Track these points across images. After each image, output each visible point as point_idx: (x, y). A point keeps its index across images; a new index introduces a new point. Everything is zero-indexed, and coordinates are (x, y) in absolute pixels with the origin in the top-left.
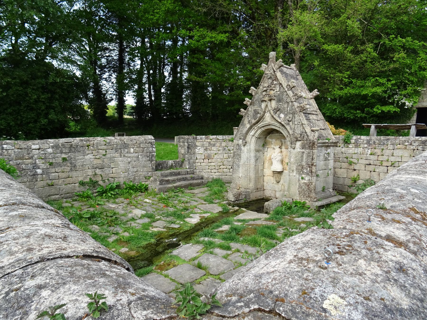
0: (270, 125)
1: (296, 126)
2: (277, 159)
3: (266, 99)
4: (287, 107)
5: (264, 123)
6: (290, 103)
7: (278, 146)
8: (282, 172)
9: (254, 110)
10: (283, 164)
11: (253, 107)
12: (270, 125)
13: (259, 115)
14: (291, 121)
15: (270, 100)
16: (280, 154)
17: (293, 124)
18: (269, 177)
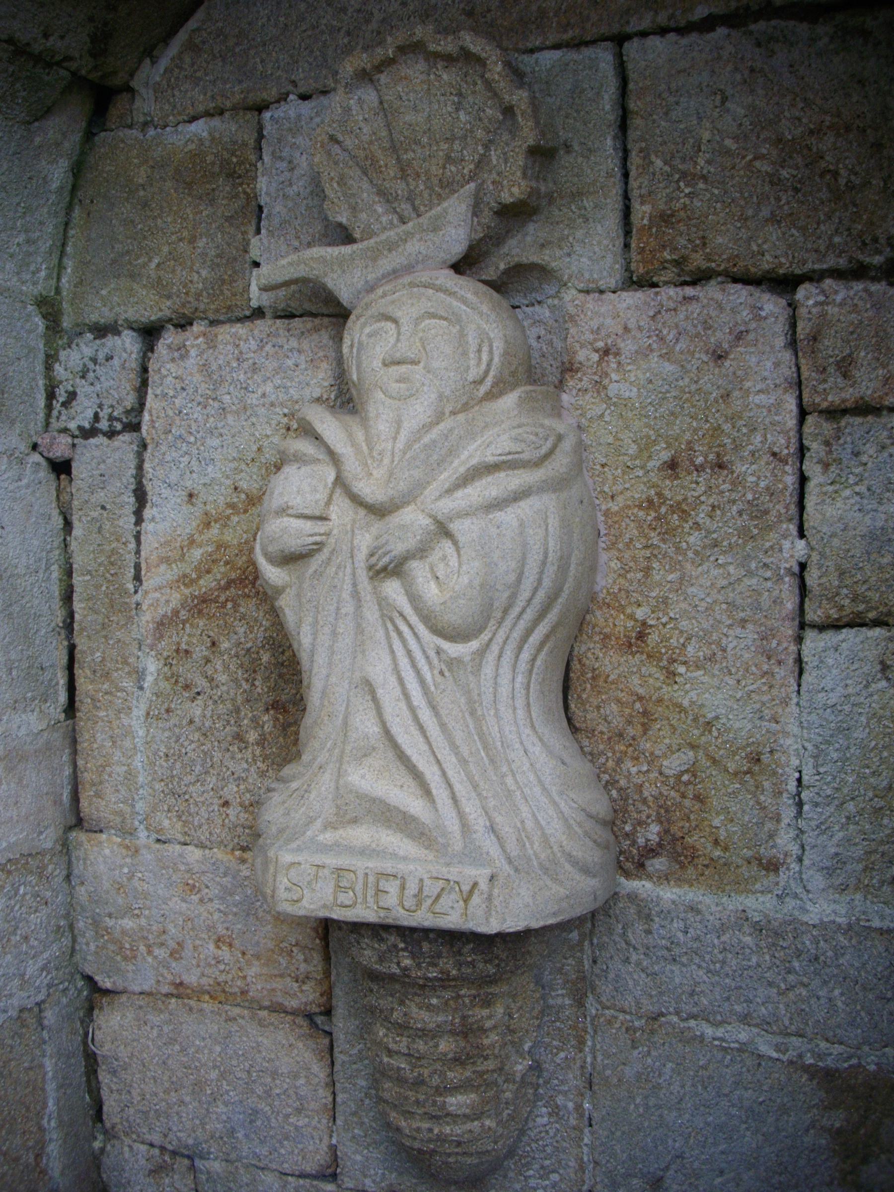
2: (446, 581)
7: (454, 225)
8: (586, 927)
10: (606, 712)
16: (506, 424)
18: (201, 1028)
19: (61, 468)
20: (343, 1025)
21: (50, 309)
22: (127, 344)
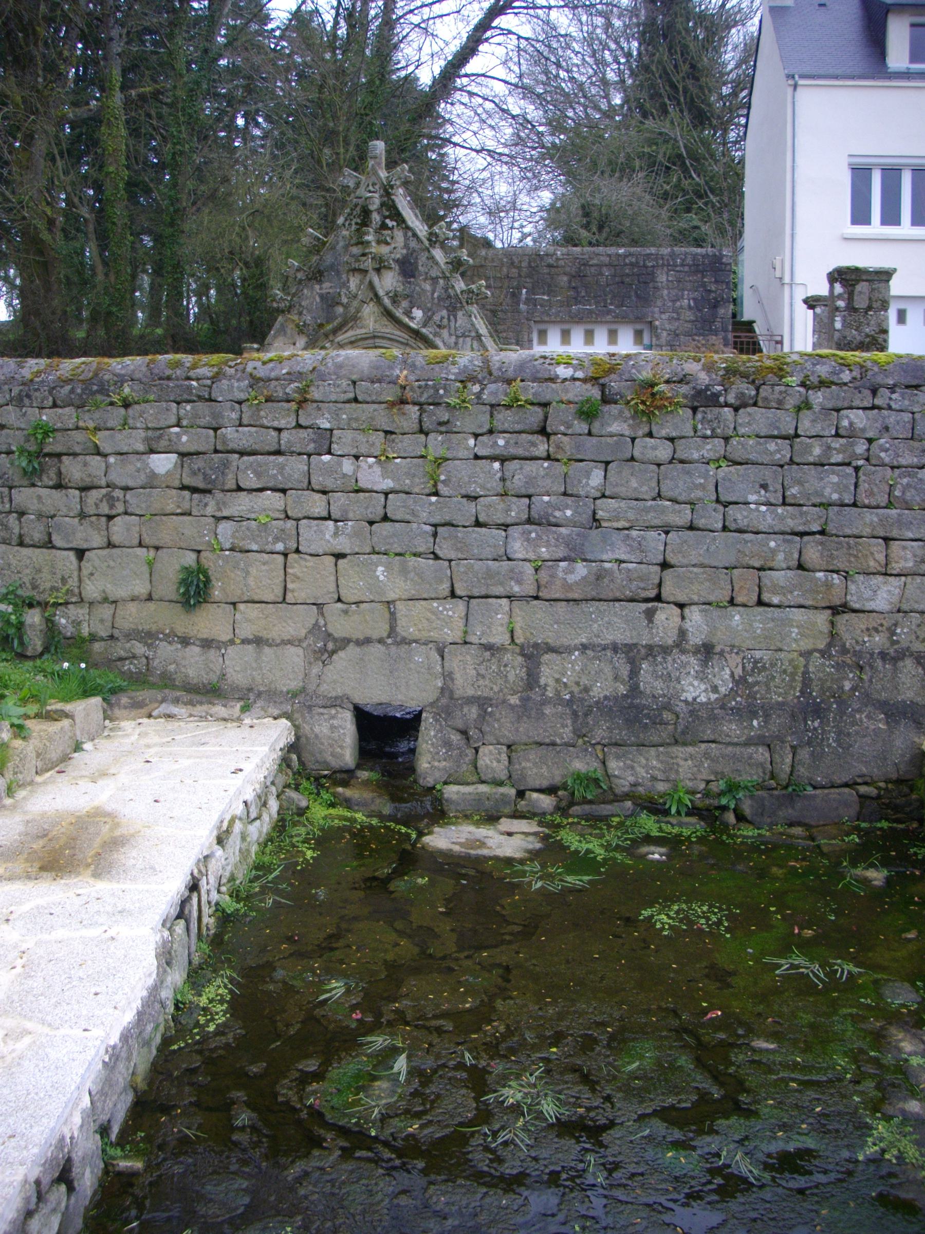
0: (374, 337)
1: (461, 340)
3: (368, 264)
4: (433, 292)
5: (359, 332)
6: (441, 281)
9: (322, 296)
11: (317, 287)
12: (374, 337)
13: (340, 310)
14: (445, 327)
15: (378, 270)
17: (450, 335)
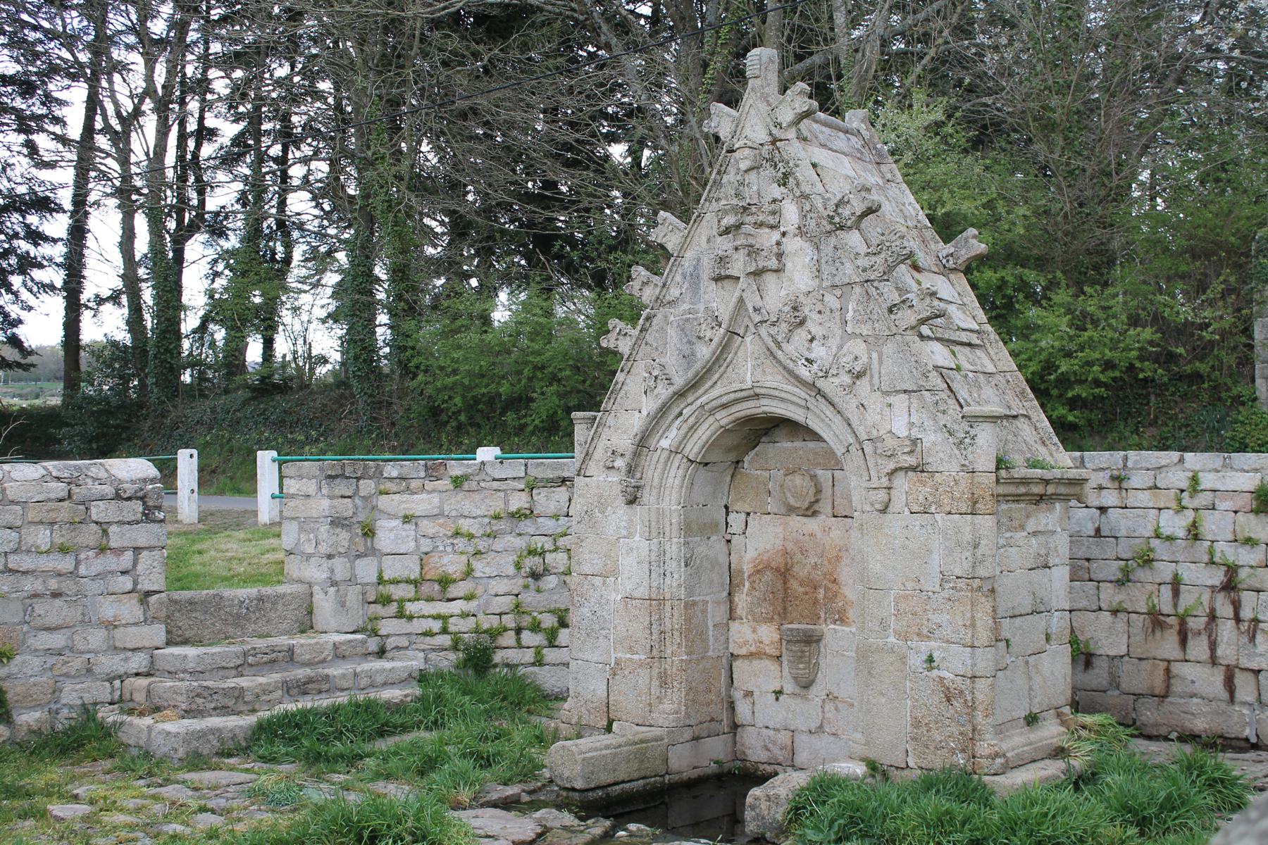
19: (729, 541)
20: (784, 659)
21: (726, 507)
22: (743, 516)
